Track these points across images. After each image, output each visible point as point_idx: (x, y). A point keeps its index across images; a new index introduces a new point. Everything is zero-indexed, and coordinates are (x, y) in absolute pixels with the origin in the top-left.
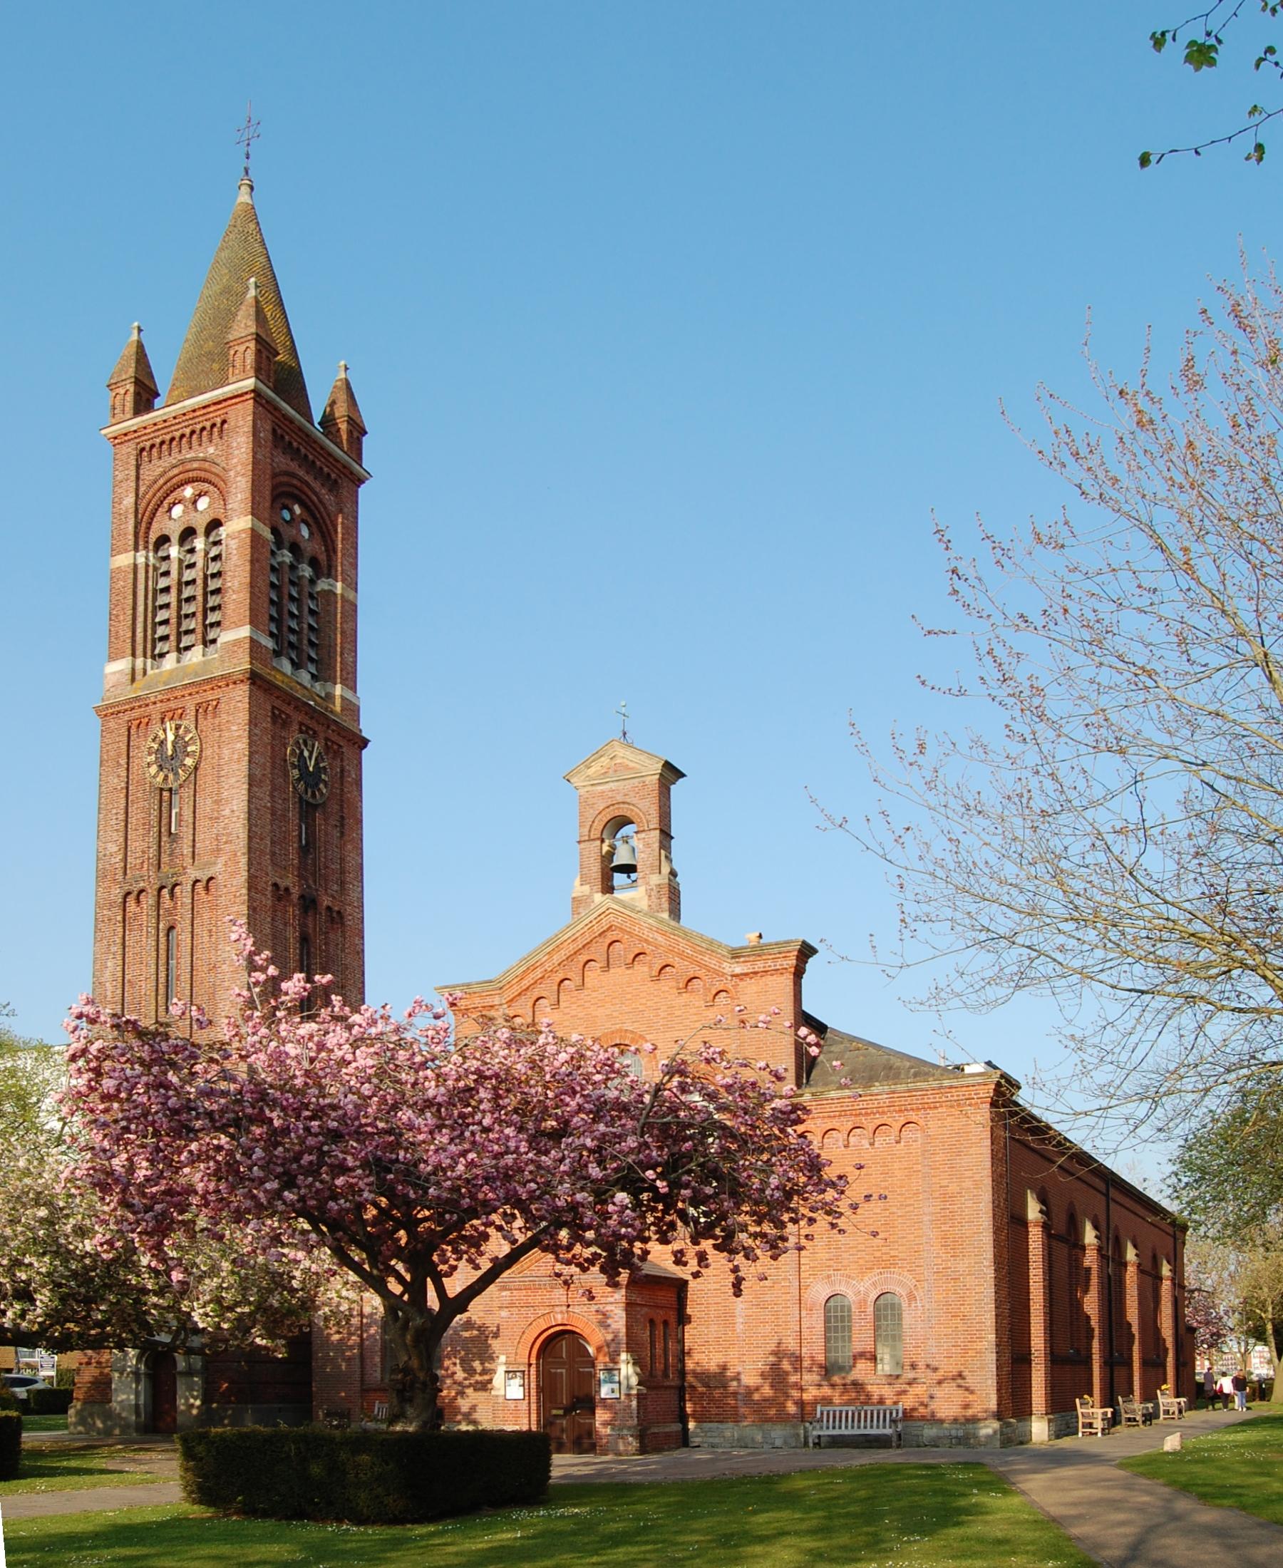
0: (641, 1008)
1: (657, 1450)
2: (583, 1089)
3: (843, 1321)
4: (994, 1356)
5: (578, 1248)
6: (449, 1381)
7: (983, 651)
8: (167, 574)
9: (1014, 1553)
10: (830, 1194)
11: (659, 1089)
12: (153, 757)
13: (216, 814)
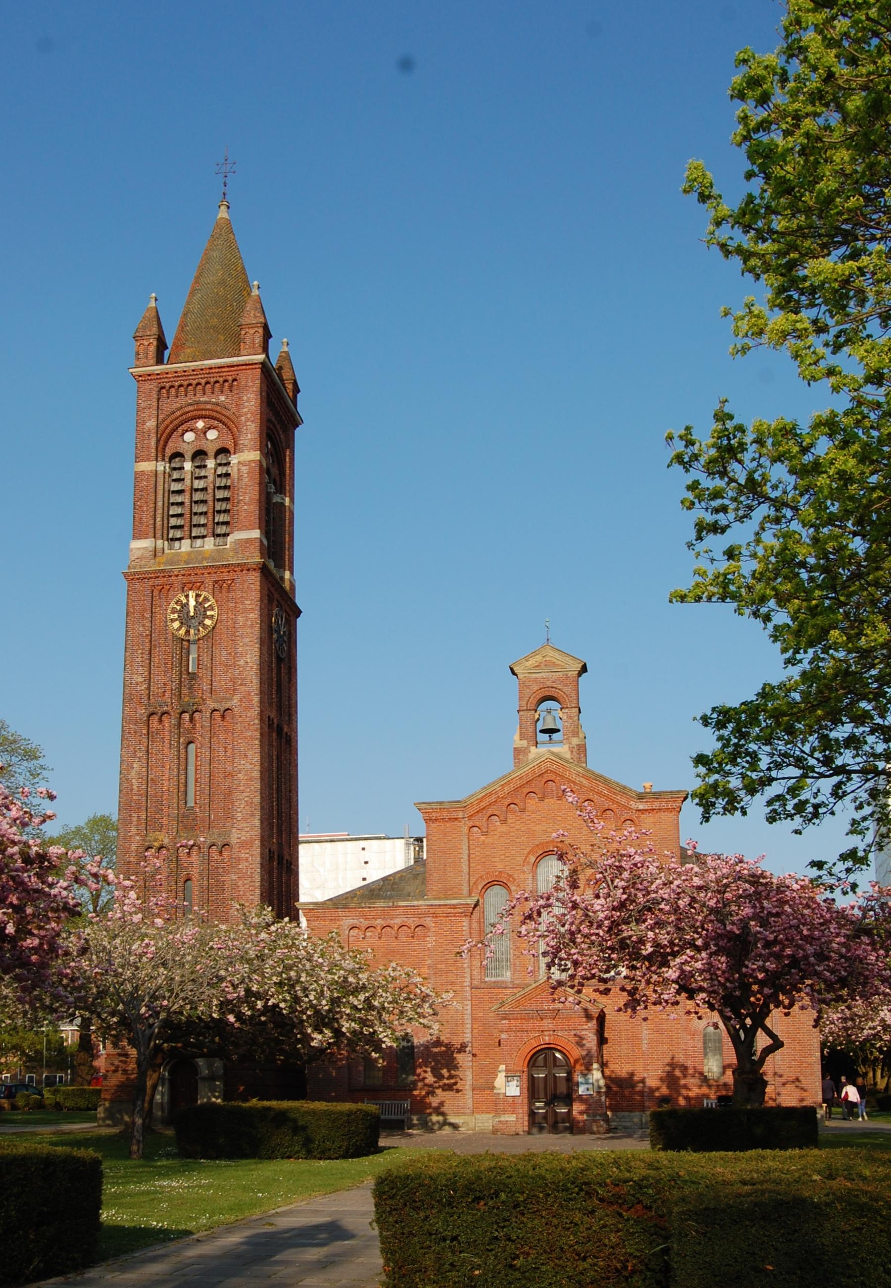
0: (568, 827)
12: (176, 616)
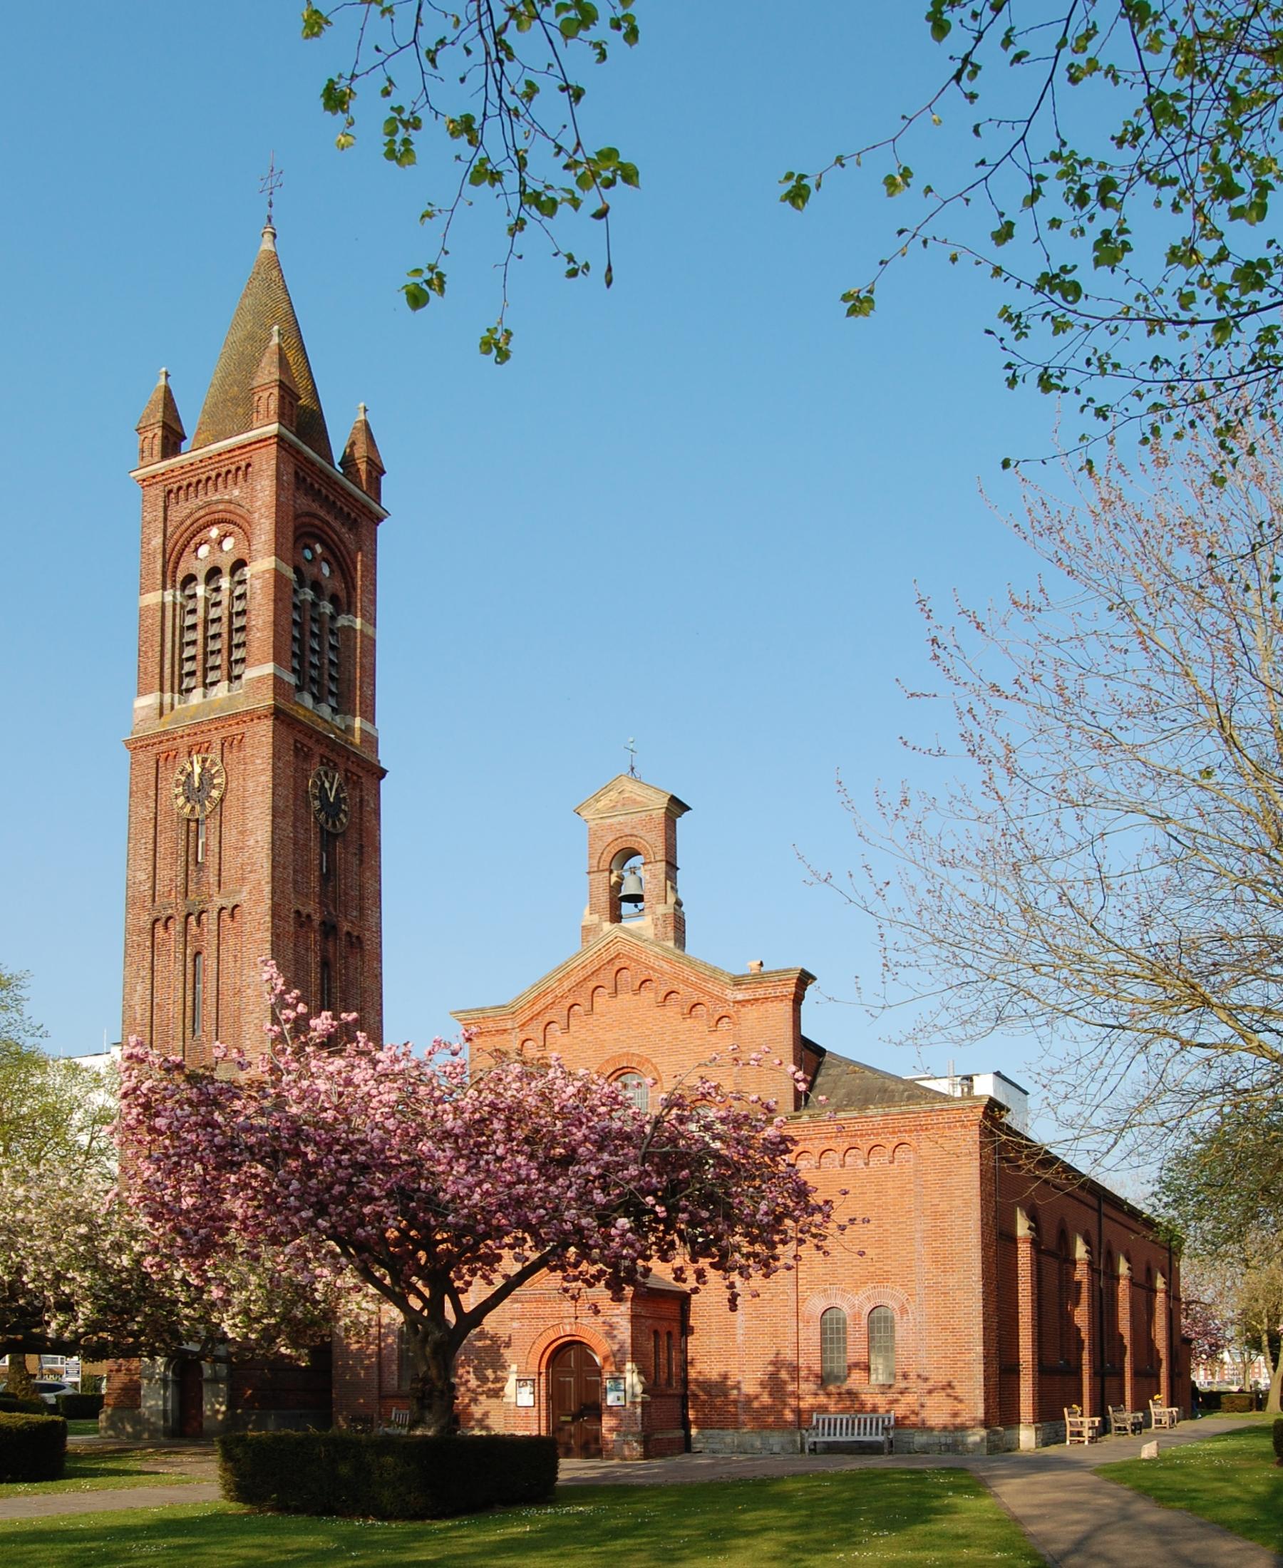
0: (648, 1032)
1: (661, 1455)
2: (589, 1120)
3: (838, 1333)
4: (982, 1367)
5: (584, 1266)
6: (462, 1389)
7: (964, 709)
8: (193, 611)
9: (969, 1546)
10: (818, 1218)
11: (658, 1122)
12: (181, 789)
13: (241, 844)
